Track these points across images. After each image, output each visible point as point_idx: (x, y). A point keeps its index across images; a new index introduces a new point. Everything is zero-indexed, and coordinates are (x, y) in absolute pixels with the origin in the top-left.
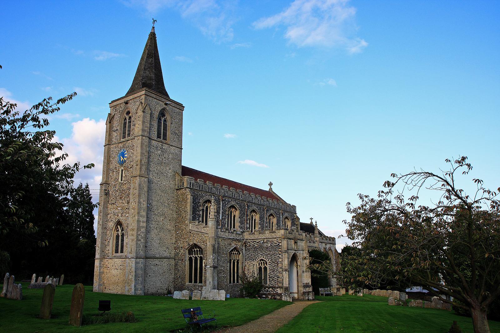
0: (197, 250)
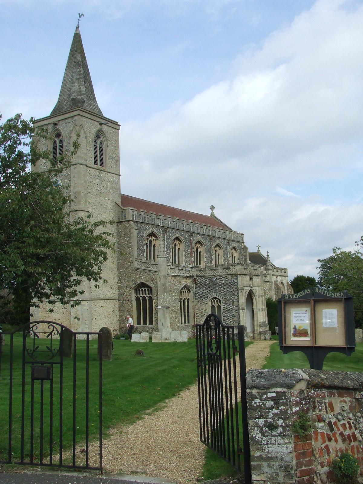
0: (145, 290)
